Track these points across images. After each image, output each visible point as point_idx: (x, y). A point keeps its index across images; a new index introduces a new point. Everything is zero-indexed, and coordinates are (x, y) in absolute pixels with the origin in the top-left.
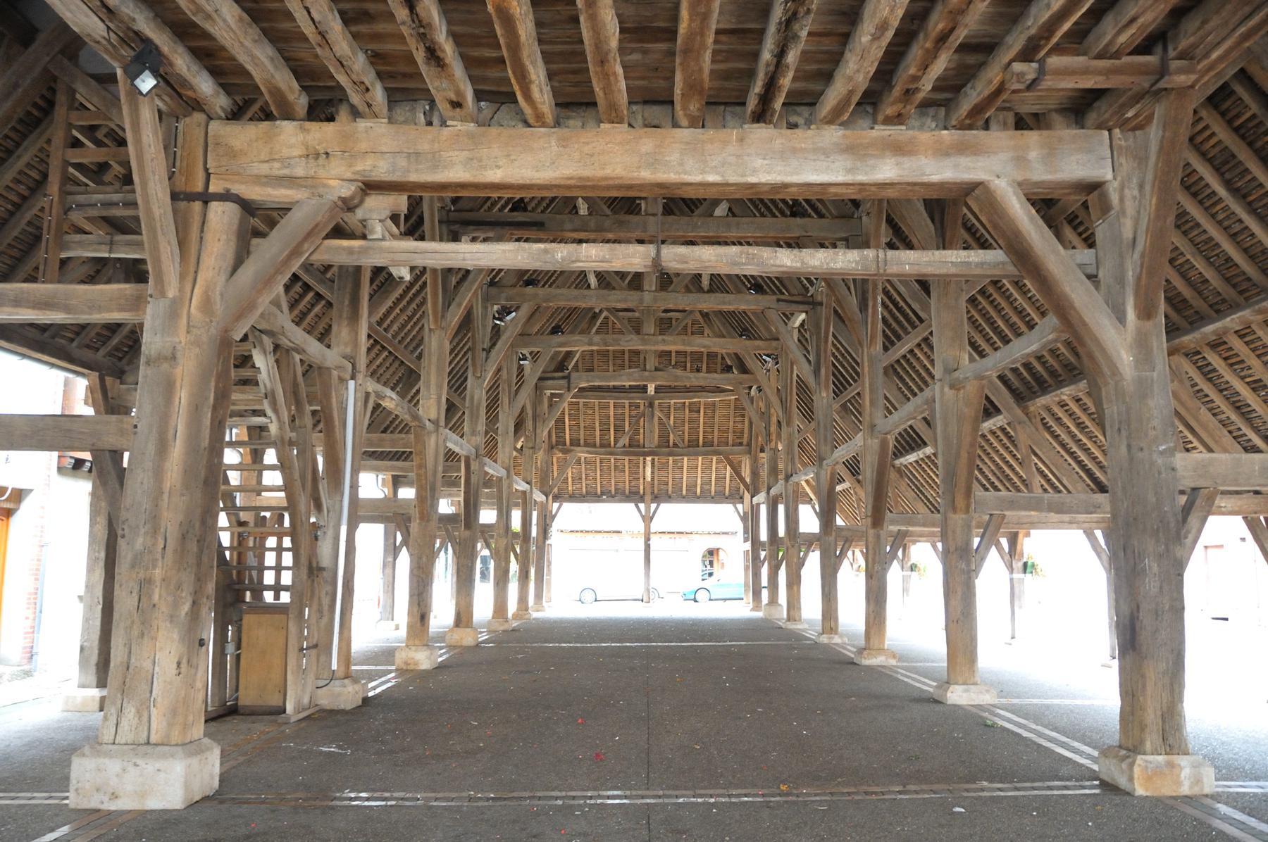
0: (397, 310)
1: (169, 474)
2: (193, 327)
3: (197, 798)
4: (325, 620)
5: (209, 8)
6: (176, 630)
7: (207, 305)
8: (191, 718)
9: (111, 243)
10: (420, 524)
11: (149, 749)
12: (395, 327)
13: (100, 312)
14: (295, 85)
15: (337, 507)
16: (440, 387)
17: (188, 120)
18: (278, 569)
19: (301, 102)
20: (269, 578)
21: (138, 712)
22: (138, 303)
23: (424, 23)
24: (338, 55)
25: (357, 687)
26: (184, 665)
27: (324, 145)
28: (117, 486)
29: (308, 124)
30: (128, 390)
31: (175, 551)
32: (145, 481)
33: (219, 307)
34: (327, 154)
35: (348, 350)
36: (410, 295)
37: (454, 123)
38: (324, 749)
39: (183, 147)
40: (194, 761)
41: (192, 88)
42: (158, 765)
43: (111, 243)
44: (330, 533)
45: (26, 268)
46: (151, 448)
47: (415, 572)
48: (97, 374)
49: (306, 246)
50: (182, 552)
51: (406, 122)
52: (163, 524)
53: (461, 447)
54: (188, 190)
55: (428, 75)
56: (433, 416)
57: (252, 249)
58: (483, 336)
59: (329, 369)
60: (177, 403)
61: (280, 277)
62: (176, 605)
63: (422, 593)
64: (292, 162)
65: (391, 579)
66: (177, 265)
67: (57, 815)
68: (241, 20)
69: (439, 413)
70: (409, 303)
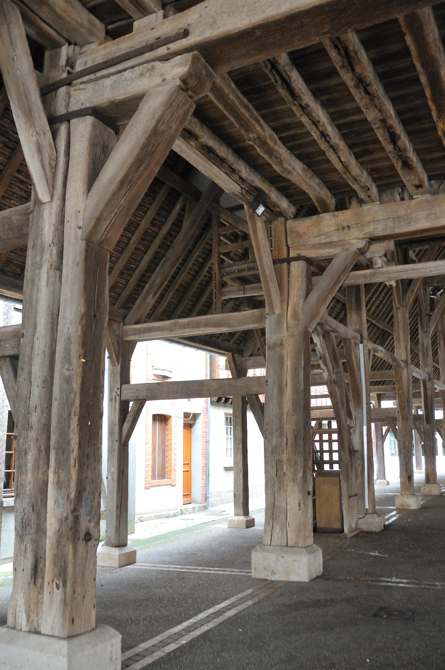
0: (374, 299)
1: (285, 405)
2: (290, 327)
3: (314, 577)
4: (359, 481)
5: (290, 168)
6: (296, 486)
7: (295, 315)
8: (307, 533)
9: (244, 290)
10: (402, 422)
11: (288, 549)
12: (373, 308)
13: (244, 325)
14: (329, 194)
15: (360, 415)
16: (406, 341)
17: (276, 222)
18: (331, 451)
19: (332, 202)
20: (326, 457)
21: (281, 529)
22: (262, 318)
23: (402, 149)
24: (354, 175)
25: (381, 519)
26: (302, 505)
27: (346, 222)
28: (260, 412)
29: (336, 213)
30: (246, 360)
31: (292, 445)
32: (274, 409)
33: (301, 316)
34: (348, 227)
35: (357, 327)
36: (381, 288)
37: (418, 196)
38: (371, 554)
39: (275, 236)
40: (311, 556)
41: (279, 207)
42: (294, 558)
43: (244, 290)
44: (358, 431)
45: (199, 305)
46: (276, 392)
47: (402, 451)
48: (231, 353)
49: (342, 277)
50: (295, 446)
51: (389, 201)
52: (285, 432)
53: (421, 375)
54: (280, 258)
55: (403, 175)
56: (404, 357)
57: (313, 283)
58: (425, 306)
59: (349, 339)
60: (286, 368)
61: (330, 295)
62: (295, 473)
63: (408, 463)
64: (331, 234)
65: (382, 455)
66: (279, 297)
67: (248, 581)
68: (304, 169)
69: (407, 357)
70: (380, 293)
